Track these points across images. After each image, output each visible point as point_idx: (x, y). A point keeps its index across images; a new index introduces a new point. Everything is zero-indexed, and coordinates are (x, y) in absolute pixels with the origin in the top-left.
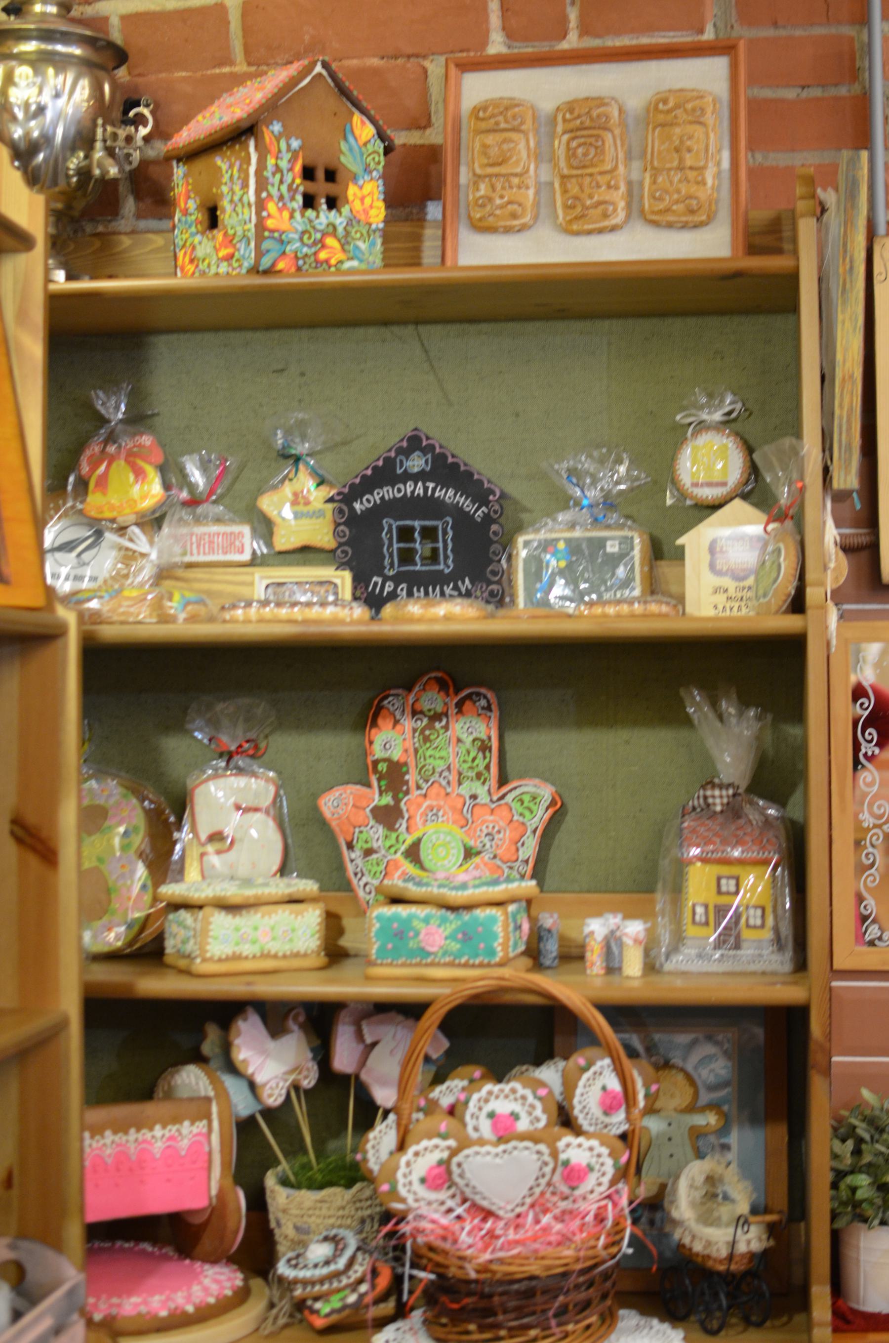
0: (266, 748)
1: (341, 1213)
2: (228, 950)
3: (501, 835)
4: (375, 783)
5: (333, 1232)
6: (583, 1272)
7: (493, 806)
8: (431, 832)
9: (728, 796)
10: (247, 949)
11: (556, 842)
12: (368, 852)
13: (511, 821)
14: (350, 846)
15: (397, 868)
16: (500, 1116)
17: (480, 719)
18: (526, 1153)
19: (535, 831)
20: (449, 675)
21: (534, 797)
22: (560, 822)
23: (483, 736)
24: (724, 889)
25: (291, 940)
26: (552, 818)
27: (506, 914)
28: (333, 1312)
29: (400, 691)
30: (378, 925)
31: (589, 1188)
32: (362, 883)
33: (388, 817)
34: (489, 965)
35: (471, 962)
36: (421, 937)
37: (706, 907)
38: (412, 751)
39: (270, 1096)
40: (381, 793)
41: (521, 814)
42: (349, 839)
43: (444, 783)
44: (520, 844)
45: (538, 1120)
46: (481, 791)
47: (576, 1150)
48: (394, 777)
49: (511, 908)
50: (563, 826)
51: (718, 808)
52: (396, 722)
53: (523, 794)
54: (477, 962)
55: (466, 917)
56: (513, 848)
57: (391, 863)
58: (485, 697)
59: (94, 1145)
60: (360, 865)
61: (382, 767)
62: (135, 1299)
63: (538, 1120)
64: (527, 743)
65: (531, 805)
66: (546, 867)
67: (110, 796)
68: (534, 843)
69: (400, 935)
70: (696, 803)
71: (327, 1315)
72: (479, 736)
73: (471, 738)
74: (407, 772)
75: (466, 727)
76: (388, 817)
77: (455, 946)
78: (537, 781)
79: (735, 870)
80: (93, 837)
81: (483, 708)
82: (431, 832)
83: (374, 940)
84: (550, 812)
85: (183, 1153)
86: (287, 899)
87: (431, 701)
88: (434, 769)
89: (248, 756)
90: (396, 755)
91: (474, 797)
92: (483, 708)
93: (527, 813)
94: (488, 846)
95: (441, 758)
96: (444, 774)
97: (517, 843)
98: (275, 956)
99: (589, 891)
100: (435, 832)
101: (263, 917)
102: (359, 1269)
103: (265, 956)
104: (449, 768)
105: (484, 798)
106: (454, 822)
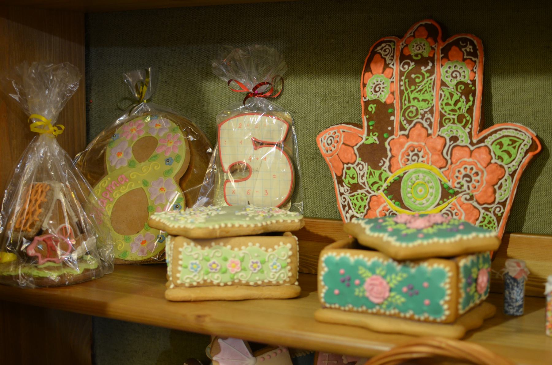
0: (283, 89)
2: (198, 278)
3: (478, 178)
4: (365, 124)
7: (472, 148)
8: (411, 171)
10: (216, 278)
11: (537, 185)
12: (355, 187)
13: (490, 163)
14: (340, 182)
15: (379, 203)
17: (464, 64)
20: (437, 22)
21: (514, 139)
22: (542, 166)
23: (467, 80)
25: (261, 271)
27: (458, 267)
29: (393, 38)
30: (326, 269)
32: (348, 216)
33: (373, 155)
34: (434, 322)
35: (416, 317)
36: (365, 286)
38: (397, 93)
40: (368, 135)
41: (500, 157)
42: (339, 175)
43: (426, 125)
44: (496, 187)
46: (462, 133)
48: (380, 117)
49: (463, 262)
50: (545, 169)
52: (386, 66)
53: (503, 137)
54: (422, 318)
55: (413, 270)
56: (490, 190)
57: (374, 198)
58: (472, 43)
60: (348, 199)
61: (372, 108)
64: (505, 88)
65: (510, 149)
66: (526, 208)
67: (161, 130)
69: (347, 281)
72: (463, 80)
73: (455, 82)
74: (393, 114)
75: (450, 71)
76: (373, 155)
77: (400, 299)
78: (518, 125)
80: (143, 164)
81: (469, 54)
82: (411, 171)
83: (322, 283)
84: (530, 155)
86: (262, 231)
87: (420, 46)
88: (417, 110)
89: (266, 97)
90: (384, 97)
91: (454, 139)
92: (469, 54)
94: (465, 187)
95: (424, 100)
96: (426, 116)
97: (495, 186)
98: (247, 285)
100: (415, 172)
101: (232, 249)
103: (235, 284)
104: (431, 111)
105: (464, 140)
106: (433, 163)
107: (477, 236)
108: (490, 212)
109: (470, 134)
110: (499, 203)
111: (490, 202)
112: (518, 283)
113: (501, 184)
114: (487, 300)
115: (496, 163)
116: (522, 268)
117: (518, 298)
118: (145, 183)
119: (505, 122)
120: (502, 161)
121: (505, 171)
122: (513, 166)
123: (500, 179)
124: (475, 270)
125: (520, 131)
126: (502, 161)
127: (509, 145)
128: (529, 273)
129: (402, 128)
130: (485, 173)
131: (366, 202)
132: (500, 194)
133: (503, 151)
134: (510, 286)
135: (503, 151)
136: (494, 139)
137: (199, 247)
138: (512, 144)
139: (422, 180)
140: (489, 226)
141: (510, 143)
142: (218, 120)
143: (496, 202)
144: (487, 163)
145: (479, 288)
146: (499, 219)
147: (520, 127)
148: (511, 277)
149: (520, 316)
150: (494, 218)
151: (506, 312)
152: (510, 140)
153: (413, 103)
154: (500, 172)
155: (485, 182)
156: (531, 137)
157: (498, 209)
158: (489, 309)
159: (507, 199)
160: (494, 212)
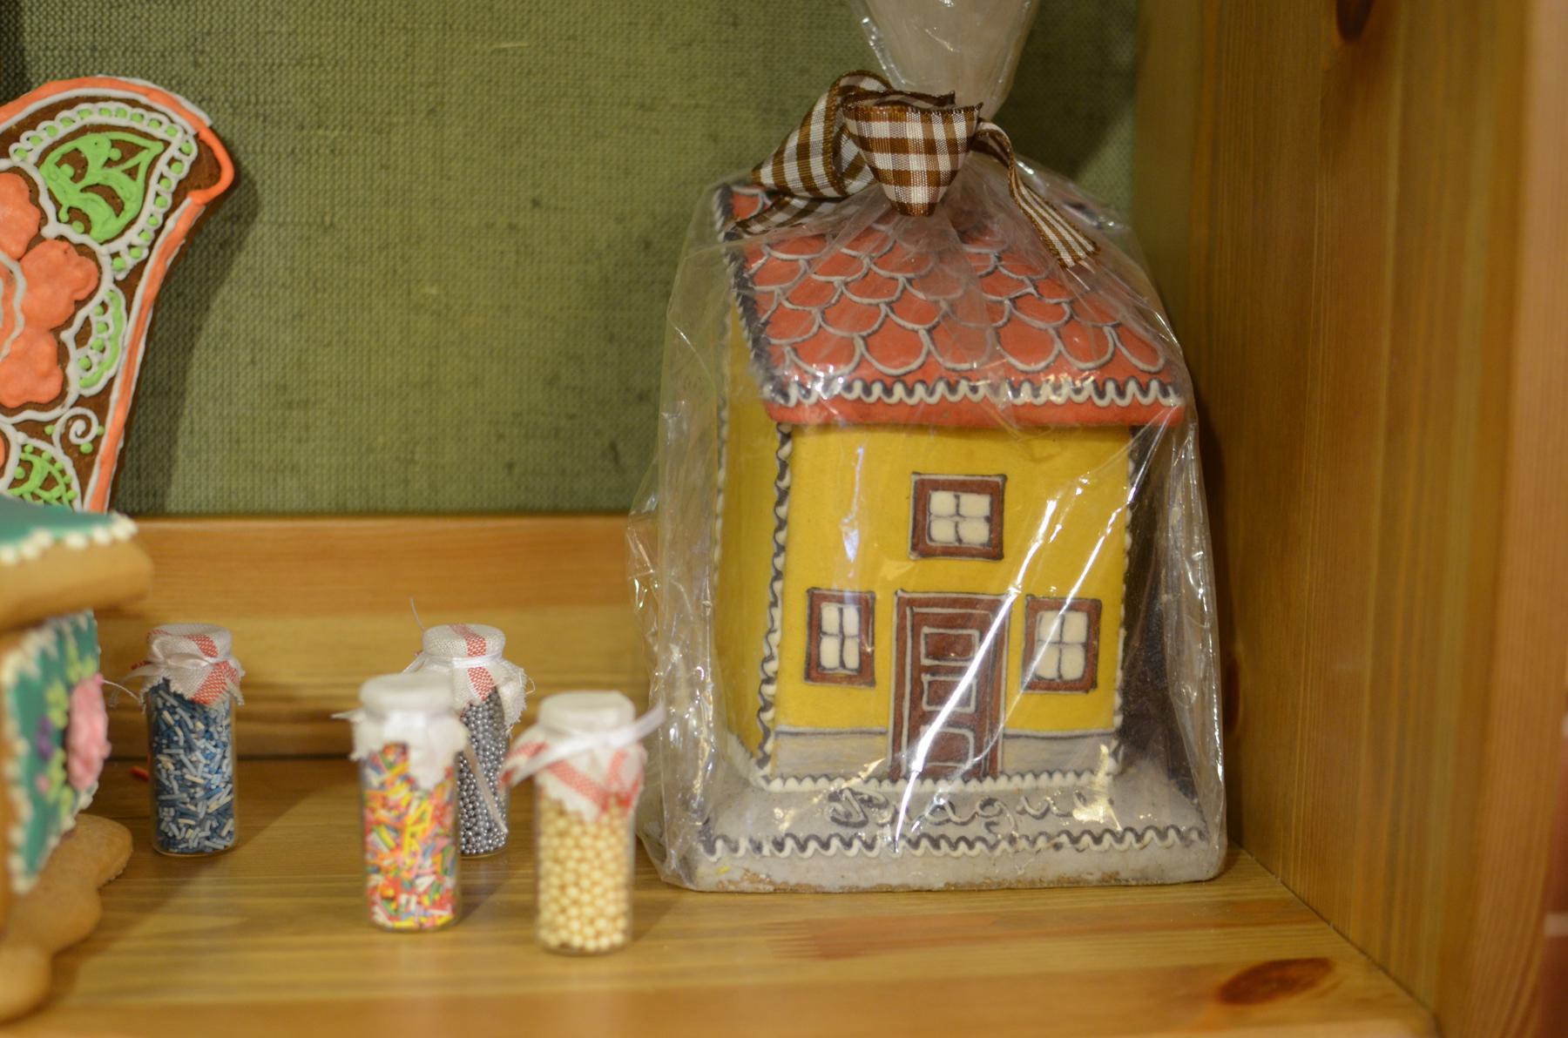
9: (952, 145)
11: (214, 323)
13: (38, 239)
19: (127, 286)
22: (229, 246)
24: (941, 532)
26: (196, 231)
37: (867, 608)
41: (77, 215)
44: (67, 336)
50: (243, 259)
51: (919, 195)
53: (83, 131)
56: (46, 348)
65: (116, 178)
66: (175, 417)
68: (129, 328)
70: (792, 173)
79: (985, 457)
84: (193, 203)
93: (98, 209)
99: (342, 512)
107: (58, 543)
108: (49, 439)
110: (81, 401)
111: (44, 399)
112: (208, 721)
113: (87, 321)
115: (62, 238)
116: (219, 659)
117: (216, 780)
119: (76, 73)
120: (87, 231)
121: (99, 268)
122: (131, 246)
123: (80, 304)
124: (56, 693)
125: (149, 108)
126: (87, 231)
127: (109, 163)
128: (242, 673)
130: (21, 282)
132: (85, 362)
133: (84, 190)
134: (180, 736)
135: (84, 190)
136: (48, 142)
138: (123, 160)
140: (45, 495)
141: (116, 154)
143: (71, 397)
144: (25, 238)
145: (77, 768)
146: (84, 465)
147: (148, 92)
148: (179, 697)
149: (227, 850)
150: (65, 462)
151: (170, 842)
152: (115, 144)
154: (79, 274)
155: (20, 319)
156: (192, 132)
157: (79, 426)
158: (111, 845)
159: (111, 381)
160: (64, 437)
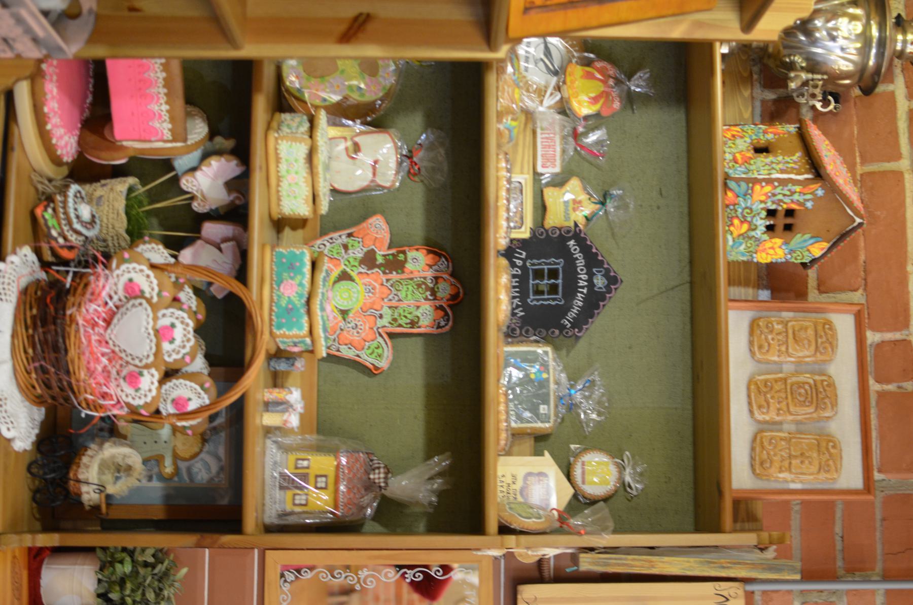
1: (110, 226)
2: (283, 154)
4: (390, 252)
5: (97, 221)
6: (70, 384)
10: (283, 167)
11: (351, 370)
12: (346, 247)
14: (350, 235)
15: (335, 266)
16: (172, 331)
18: (148, 348)
21: (381, 356)
23: (421, 323)
24: (319, 479)
25: (289, 196)
26: (367, 367)
28: (46, 220)
29: (451, 269)
31: (125, 389)
32: (325, 243)
33: (369, 260)
34: (271, 325)
36: (290, 281)
37: (308, 468)
38: (412, 276)
39: (187, 181)
40: (384, 256)
41: (369, 347)
43: (390, 297)
45: (170, 356)
46: (385, 322)
47: (149, 381)
48: (395, 264)
49: (308, 340)
50: (361, 375)
51: (372, 476)
52: (430, 266)
54: (273, 317)
55: (303, 311)
56: (347, 342)
58: (446, 325)
59: (157, 66)
61: (401, 257)
62: (55, 91)
63: (170, 356)
64: (416, 348)
65: (375, 354)
69: (292, 267)
71: (43, 217)
73: (419, 315)
74: (398, 273)
76: (369, 260)
77: (284, 303)
78: (391, 358)
79: (331, 487)
84: (371, 366)
85: (151, 124)
87: (444, 290)
90: (409, 266)
91: (381, 316)
93: (370, 351)
95: (407, 295)
98: (278, 185)
99: (318, 391)
102: (73, 238)
104: (400, 300)
105: (380, 323)
109: (385, 326)
114: (278, 348)
118: (343, 71)
119: (393, 347)
129: (388, 280)
131: (336, 256)
137: (305, 156)
139: (353, 295)
142: (392, 131)
153: (405, 287)
